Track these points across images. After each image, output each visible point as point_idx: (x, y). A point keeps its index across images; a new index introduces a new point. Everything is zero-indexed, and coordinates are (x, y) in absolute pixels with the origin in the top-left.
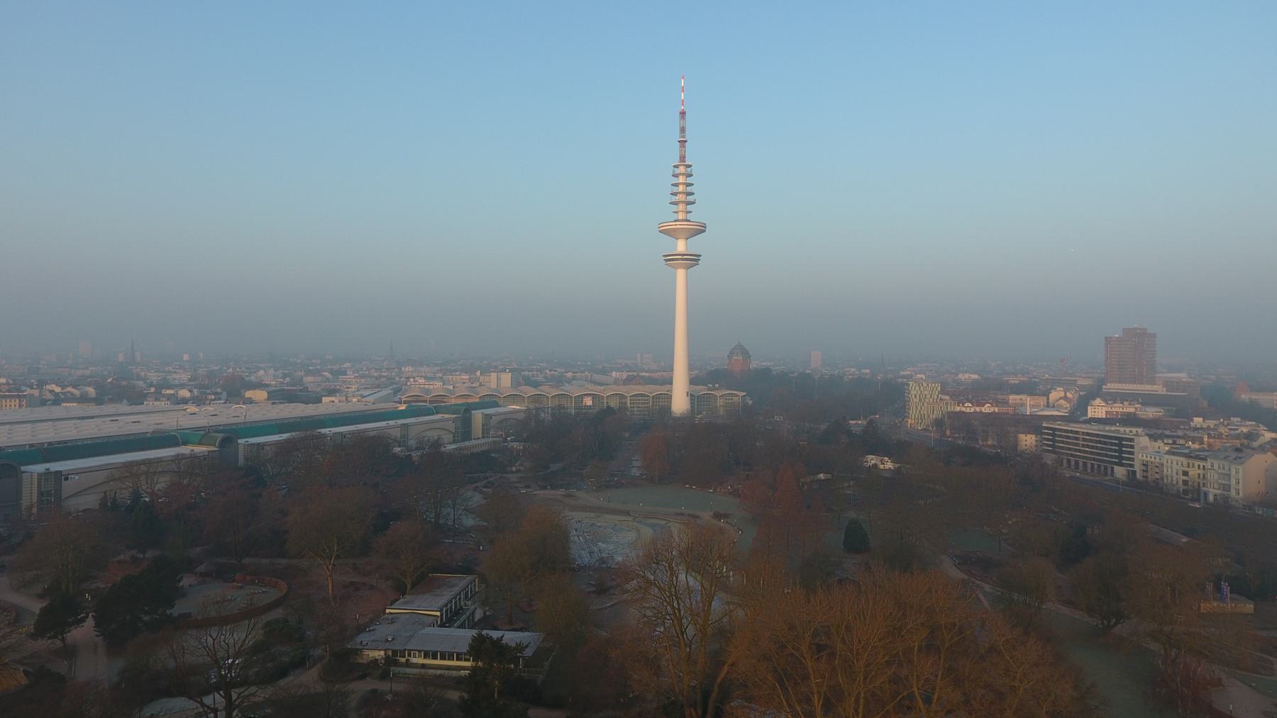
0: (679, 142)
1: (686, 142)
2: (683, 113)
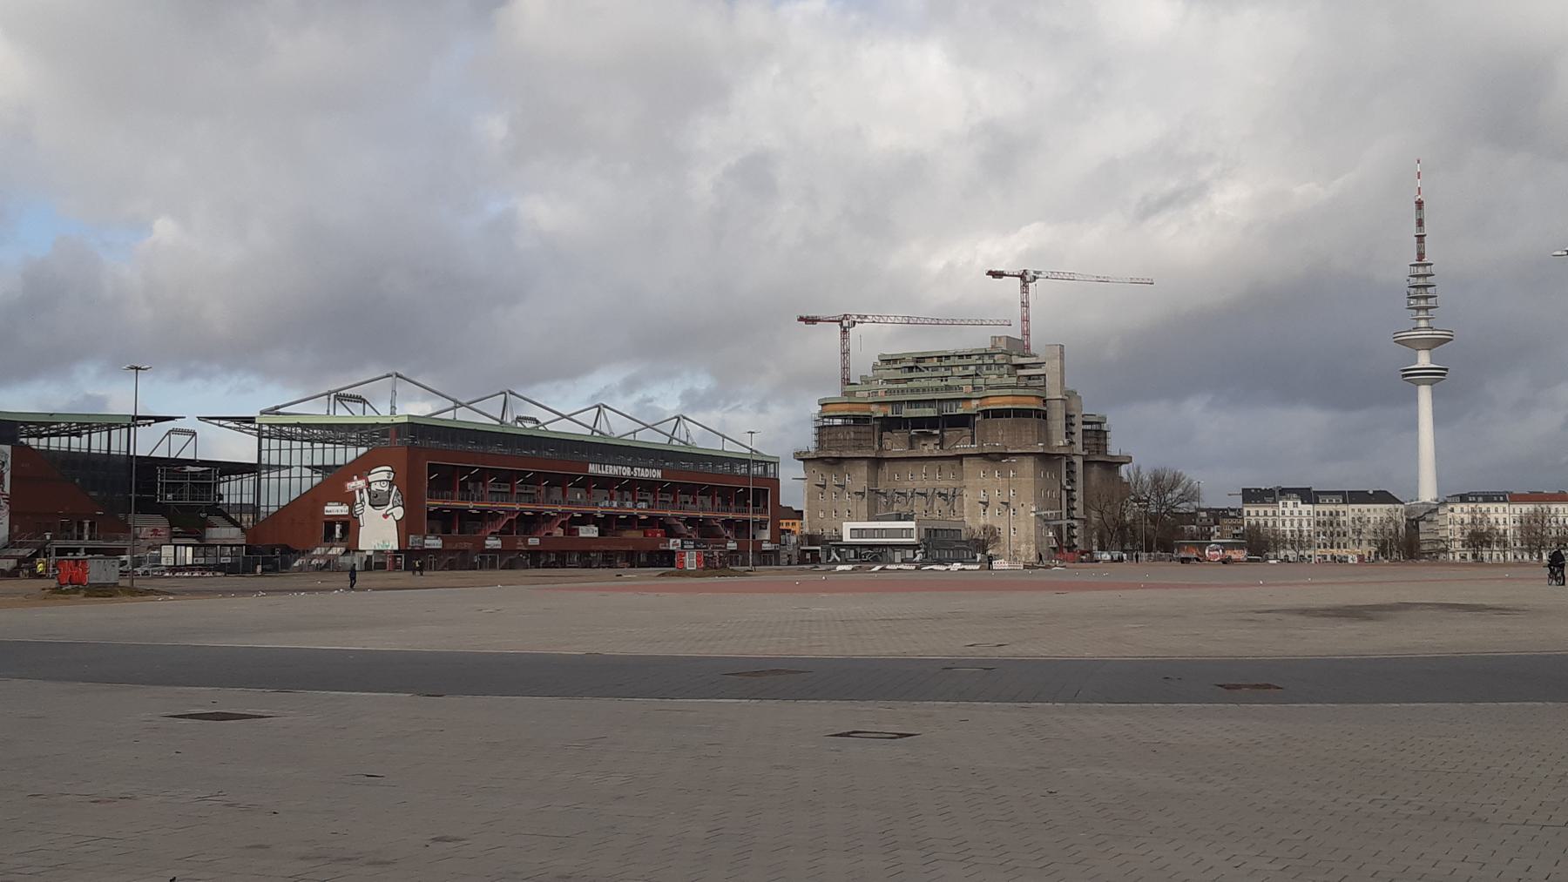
0: (1416, 236)
1: (1425, 235)
2: (1420, 204)
